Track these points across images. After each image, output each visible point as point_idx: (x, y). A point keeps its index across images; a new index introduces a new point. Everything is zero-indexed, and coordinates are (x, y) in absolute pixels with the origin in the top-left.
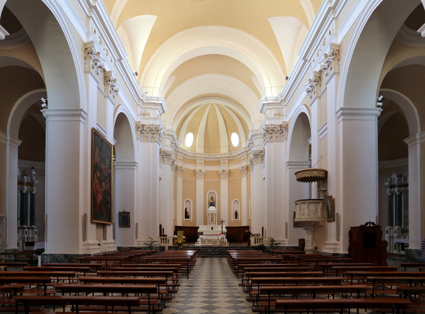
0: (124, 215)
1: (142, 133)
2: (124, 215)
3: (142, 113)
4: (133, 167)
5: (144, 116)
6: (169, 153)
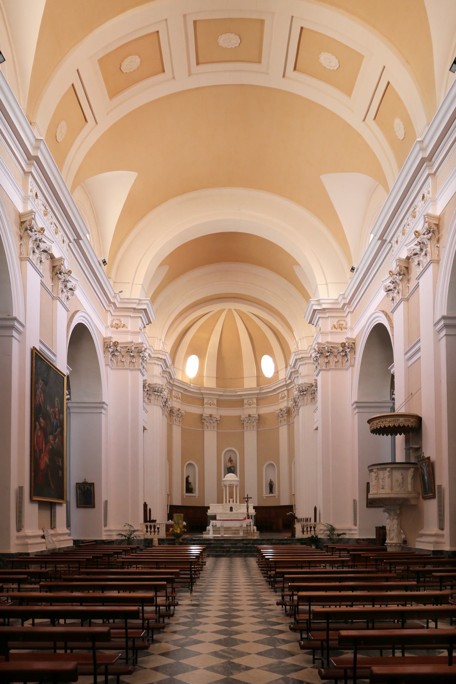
0: (84, 488)
1: (113, 355)
2: (84, 488)
3: (114, 324)
4: (99, 411)
5: (117, 328)
6: (158, 388)
